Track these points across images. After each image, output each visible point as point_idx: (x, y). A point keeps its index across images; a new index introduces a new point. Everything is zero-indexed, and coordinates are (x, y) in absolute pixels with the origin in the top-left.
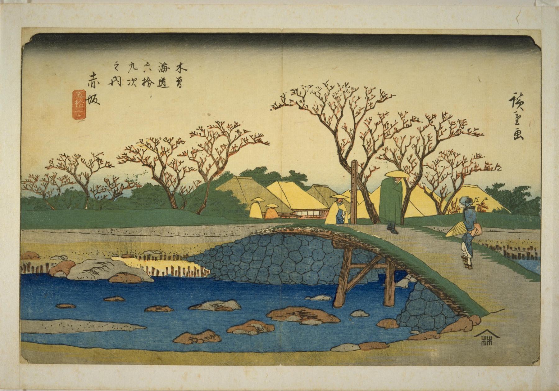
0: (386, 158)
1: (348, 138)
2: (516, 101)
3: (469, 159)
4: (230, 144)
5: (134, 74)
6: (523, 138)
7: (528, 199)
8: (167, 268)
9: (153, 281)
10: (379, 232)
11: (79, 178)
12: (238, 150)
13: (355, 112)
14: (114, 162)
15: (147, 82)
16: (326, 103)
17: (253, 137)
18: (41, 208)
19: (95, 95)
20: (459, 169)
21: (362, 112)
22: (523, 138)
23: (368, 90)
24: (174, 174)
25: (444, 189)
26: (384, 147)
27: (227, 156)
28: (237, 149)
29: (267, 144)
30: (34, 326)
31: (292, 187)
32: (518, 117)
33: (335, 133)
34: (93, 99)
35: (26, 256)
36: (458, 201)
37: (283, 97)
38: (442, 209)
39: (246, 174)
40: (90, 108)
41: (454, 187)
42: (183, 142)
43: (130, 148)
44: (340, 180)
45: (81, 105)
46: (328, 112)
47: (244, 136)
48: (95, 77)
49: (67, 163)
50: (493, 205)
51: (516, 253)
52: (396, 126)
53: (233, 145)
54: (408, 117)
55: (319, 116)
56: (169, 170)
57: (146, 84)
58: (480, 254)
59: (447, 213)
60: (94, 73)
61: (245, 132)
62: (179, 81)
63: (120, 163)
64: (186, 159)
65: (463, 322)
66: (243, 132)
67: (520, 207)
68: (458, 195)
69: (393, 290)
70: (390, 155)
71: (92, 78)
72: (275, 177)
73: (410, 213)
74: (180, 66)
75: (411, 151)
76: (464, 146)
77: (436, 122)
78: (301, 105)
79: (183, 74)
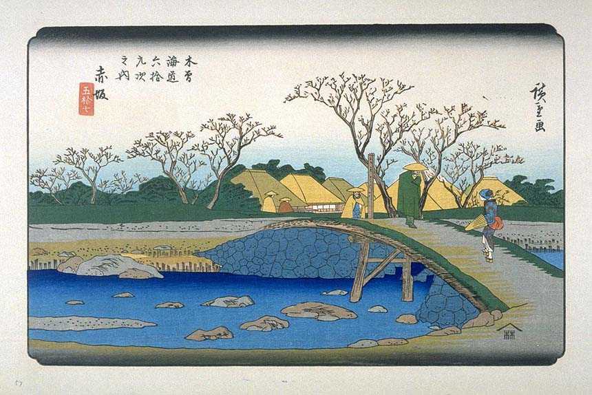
0: (403, 150)
1: (364, 131)
2: (539, 92)
3: (489, 152)
4: (241, 138)
5: (141, 68)
6: (544, 130)
7: (551, 192)
8: (178, 264)
9: (162, 277)
10: (398, 224)
11: (86, 172)
12: (250, 143)
13: (372, 104)
14: (123, 156)
15: (156, 76)
16: (342, 95)
17: (266, 129)
18: (45, 206)
19: (103, 90)
20: (479, 162)
21: (380, 103)
22: (544, 130)
23: (385, 81)
24: (185, 169)
25: (463, 182)
26: (401, 140)
27: (240, 148)
28: (248, 141)
29: (279, 136)
30: (38, 323)
31: (307, 180)
32: (540, 108)
33: (351, 125)
34: (101, 94)
35: (33, 250)
36: (478, 194)
37: (298, 89)
38: (462, 203)
39: (258, 167)
40: (98, 103)
41: (475, 181)
42: (193, 136)
43: (139, 143)
44: (358, 174)
45: (89, 98)
46: (344, 103)
47: (256, 129)
48: (103, 71)
49: (74, 157)
50: (513, 198)
51: (538, 247)
52: (414, 119)
53: (244, 138)
54: (426, 109)
55: (335, 109)
56: (179, 164)
57: (155, 78)
58: (501, 248)
59: (467, 207)
60: (101, 67)
61: (257, 124)
62: (188, 74)
63: (129, 158)
64: (197, 153)
65: (484, 317)
66: (255, 125)
67: (543, 201)
68: (478, 189)
69: (412, 283)
70: (408, 148)
71: (99, 73)
72: (288, 170)
73: (429, 206)
74: (189, 60)
75: (429, 145)
76: (483, 137)
77: (455, 114)
78: (317, 97)
79: (193, 68)
